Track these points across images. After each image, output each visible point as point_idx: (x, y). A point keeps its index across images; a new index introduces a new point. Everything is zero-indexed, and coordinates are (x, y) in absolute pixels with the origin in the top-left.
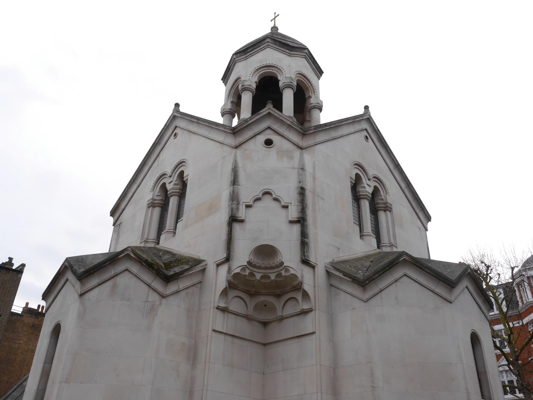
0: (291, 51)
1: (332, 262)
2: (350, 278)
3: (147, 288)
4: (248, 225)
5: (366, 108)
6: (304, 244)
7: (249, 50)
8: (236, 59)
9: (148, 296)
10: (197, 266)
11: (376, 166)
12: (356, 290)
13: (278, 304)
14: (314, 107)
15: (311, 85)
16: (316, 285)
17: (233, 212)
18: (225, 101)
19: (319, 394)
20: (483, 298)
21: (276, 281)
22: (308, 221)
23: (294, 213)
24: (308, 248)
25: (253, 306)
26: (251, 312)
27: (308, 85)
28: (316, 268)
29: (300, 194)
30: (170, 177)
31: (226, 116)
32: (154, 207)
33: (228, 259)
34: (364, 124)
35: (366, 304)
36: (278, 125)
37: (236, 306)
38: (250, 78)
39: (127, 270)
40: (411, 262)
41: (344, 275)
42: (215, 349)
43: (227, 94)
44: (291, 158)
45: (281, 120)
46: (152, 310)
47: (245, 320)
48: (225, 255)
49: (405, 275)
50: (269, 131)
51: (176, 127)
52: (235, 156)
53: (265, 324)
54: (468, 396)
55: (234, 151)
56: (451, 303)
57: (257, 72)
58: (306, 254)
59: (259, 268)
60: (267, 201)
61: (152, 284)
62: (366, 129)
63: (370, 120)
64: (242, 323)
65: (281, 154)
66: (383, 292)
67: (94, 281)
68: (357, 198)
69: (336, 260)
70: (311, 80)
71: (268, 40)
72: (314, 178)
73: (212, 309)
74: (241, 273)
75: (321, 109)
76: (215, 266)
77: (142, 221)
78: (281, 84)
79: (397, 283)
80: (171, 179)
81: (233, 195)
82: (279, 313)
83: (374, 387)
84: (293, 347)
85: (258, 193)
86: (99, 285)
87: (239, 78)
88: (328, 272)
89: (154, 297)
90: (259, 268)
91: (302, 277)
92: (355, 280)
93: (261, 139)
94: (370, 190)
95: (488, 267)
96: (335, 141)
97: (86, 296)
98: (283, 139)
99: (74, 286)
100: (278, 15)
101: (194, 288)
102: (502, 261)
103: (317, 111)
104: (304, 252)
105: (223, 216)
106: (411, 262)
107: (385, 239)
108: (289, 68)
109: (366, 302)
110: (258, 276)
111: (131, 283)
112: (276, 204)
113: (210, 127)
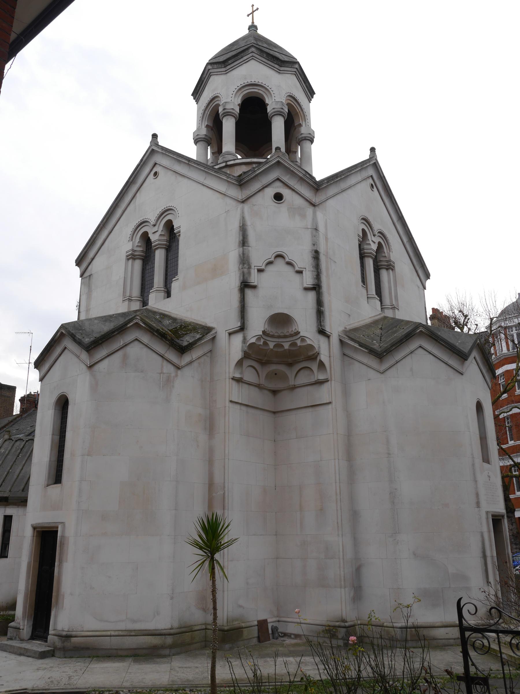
0: (281, 66)
1: (344, 331)
2: (366, 349)
3: (160, 358)
4: (261, 292)
5: (373, 150)
6: (320, 313)
7: (230, 62)
8: (211, 71)
9: (162, 367)
10: (208, 335)
11: (382, 222)
12: (372, 362)
13: (290, 373)
14: (305, 139)
15: (302, 110)
16: (332, 355)
17: (245, 277)
18: (198, 123)
19: (337, 461)
20: (487, 367)
21: (289, 350)
22: (237, 240)
23: (308, 279)
24: (324, 317)
25: (264, 375)
26: (263, 381)
27: (298, 109)
28: (331, 338)
29: (314, 258)
30: (154, 225)
31: (200, 144)
32: (134, 259)
33: (242, 328)
34: (370, 171)
35: (382, 375)
36: (288, 177)
37: (249, 376)
38: (233, 99)
39: (136, 339)
40: (427, 334)
41: (360, 346)
42: (232, 420)
43: (201, 115)
44: (303, 216)
45: (292, 171)
46: (169, 382)
47: (257, 389)
48: (239, 324)
49: (420, 347)
50: (278, 184)
51: (156, 164)
52: (243, 212)
53: (275, 392)
54: (473, 461)
55: (241, 206)
56: (462, 374)
57: (240, 92)
58: (322, 324)
59: (273, 336)
60: (280, 264)
61: (166, 355)
62: (372, 176)
63: (376, 166)
64: (254, 392)
65: (293, 211)
66: (398, 364)
67: (103, 352)
68: (362, 257)
69: (348, 328)
70: (302, 104)
71: (253, 49)
72: (327, 239)
73: (227, 380)
74: (257, 343)
75: (312, 141)
76: (227, 334)
77: (122, 275)
78: (269, 109)
79: (413, 355)
80: (155, 229)
81: (244, 257)
82: (292, 382)
83: (389, 454)
84: (307, 416)
85: (270, 255)
86: (108, 356)
87: (217, 97)
88: (341, 341)
89: (169, 369)
90: (273, 336)
91: (319, 347)
92: (372, 352)
93: (270, 192)
94: (374, 247)
95: (466, 316)
96: (344, 194)
97: (96, 367)
98: (294, 193)
99: (78, 357)
100: (257, 9)
101: (205, 357)
102: (481, 310)
103: (308, 142)
104: (321, 322)
105: (233, 280)
106: (427, 334)
107: (387, 301)
108: (278, 89)
109: (382, 373)
110: (271, 345)
111: (141, 353)
112: (288, 268)
113: (206, 172)
